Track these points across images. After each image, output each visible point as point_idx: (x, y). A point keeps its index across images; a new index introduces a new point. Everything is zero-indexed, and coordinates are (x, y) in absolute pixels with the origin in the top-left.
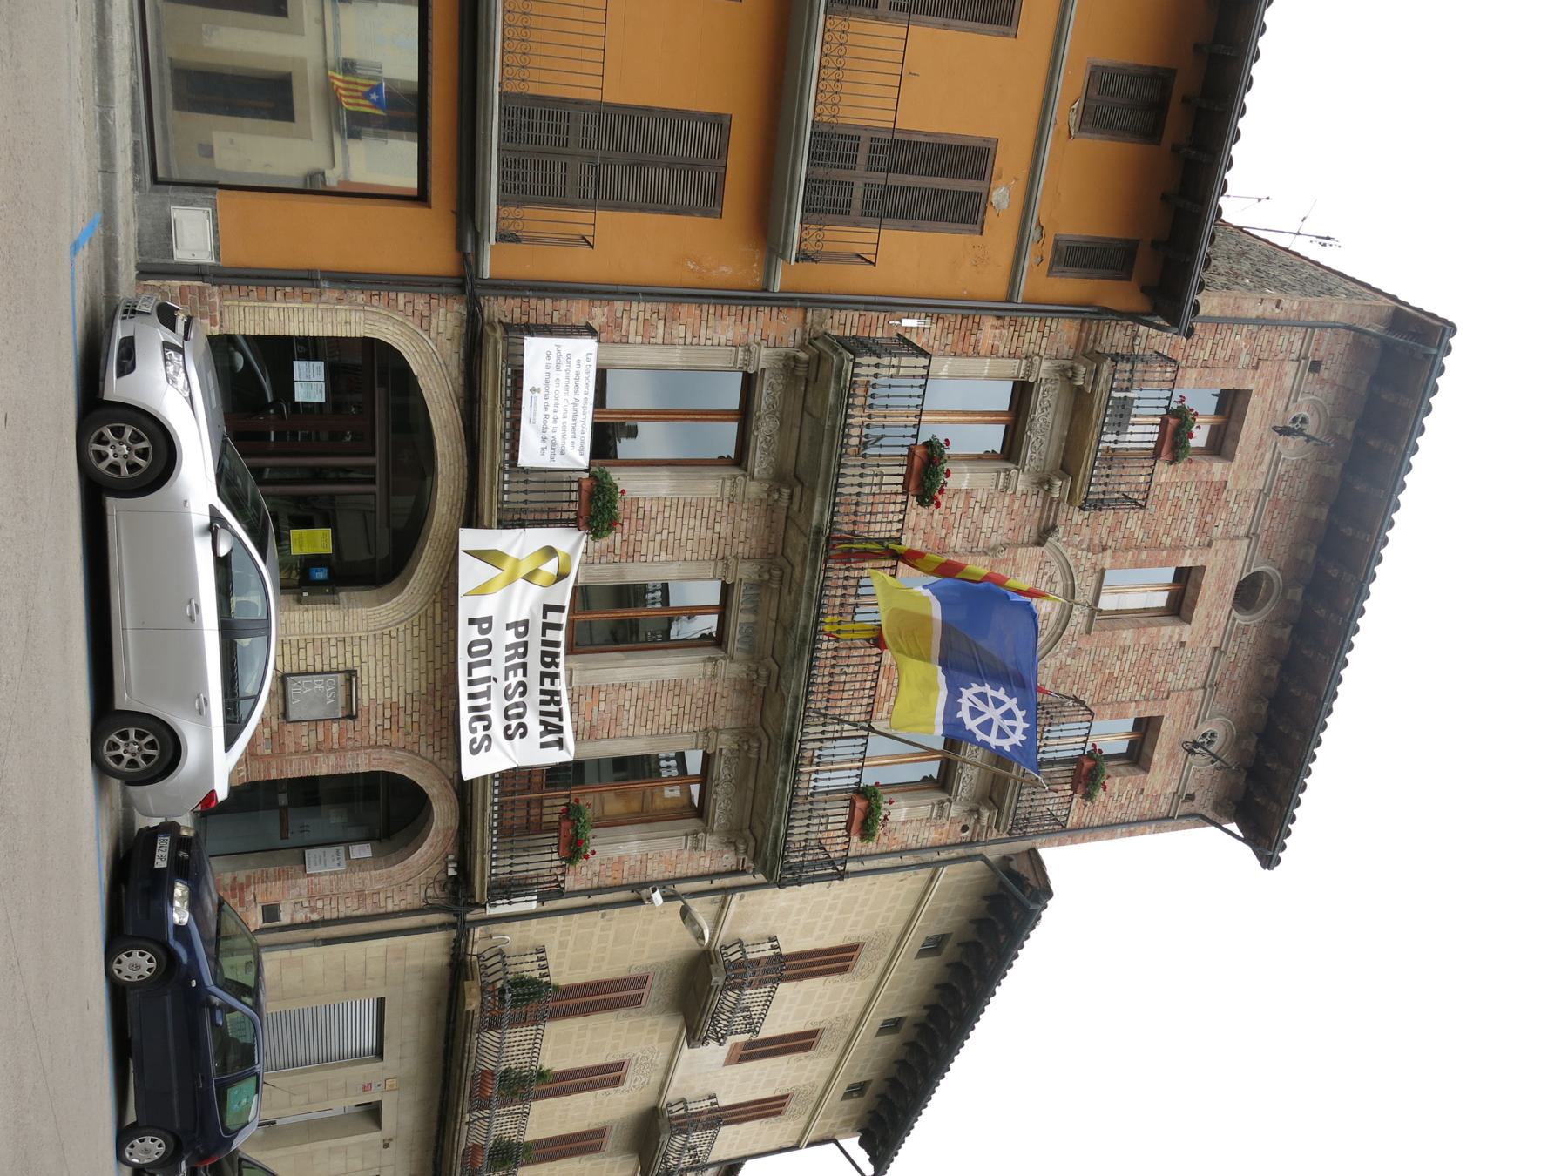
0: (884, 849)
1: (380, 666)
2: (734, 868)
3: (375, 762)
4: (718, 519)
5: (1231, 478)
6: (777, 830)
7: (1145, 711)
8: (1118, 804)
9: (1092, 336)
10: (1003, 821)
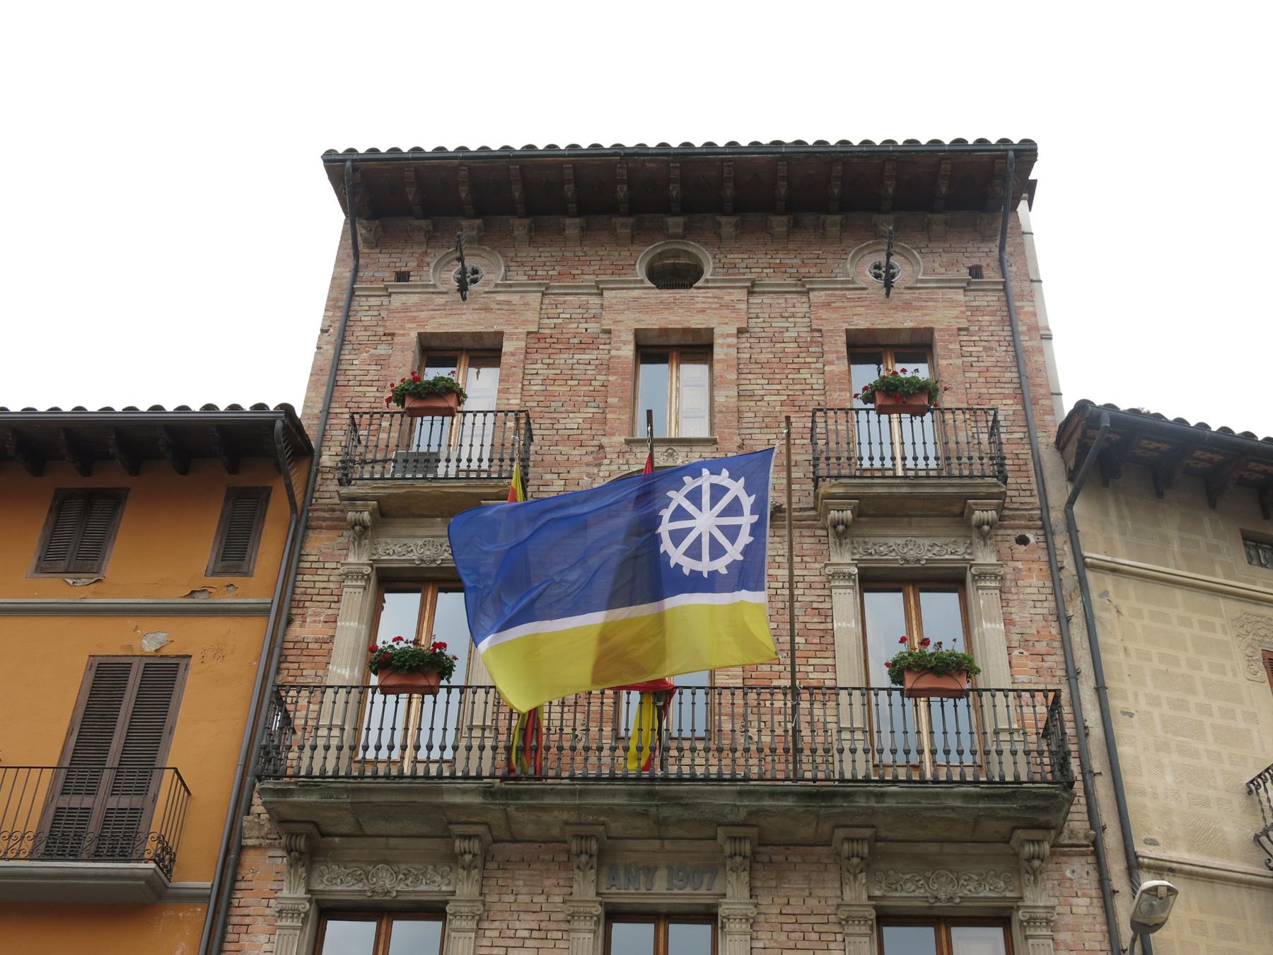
0: (1057, 644)
2: (1091, 859)
4: (511, 933)
5: (523, 330)
6: (967, 797)
8: (984, 354)
9: (326, 515)
10: (984, 490)
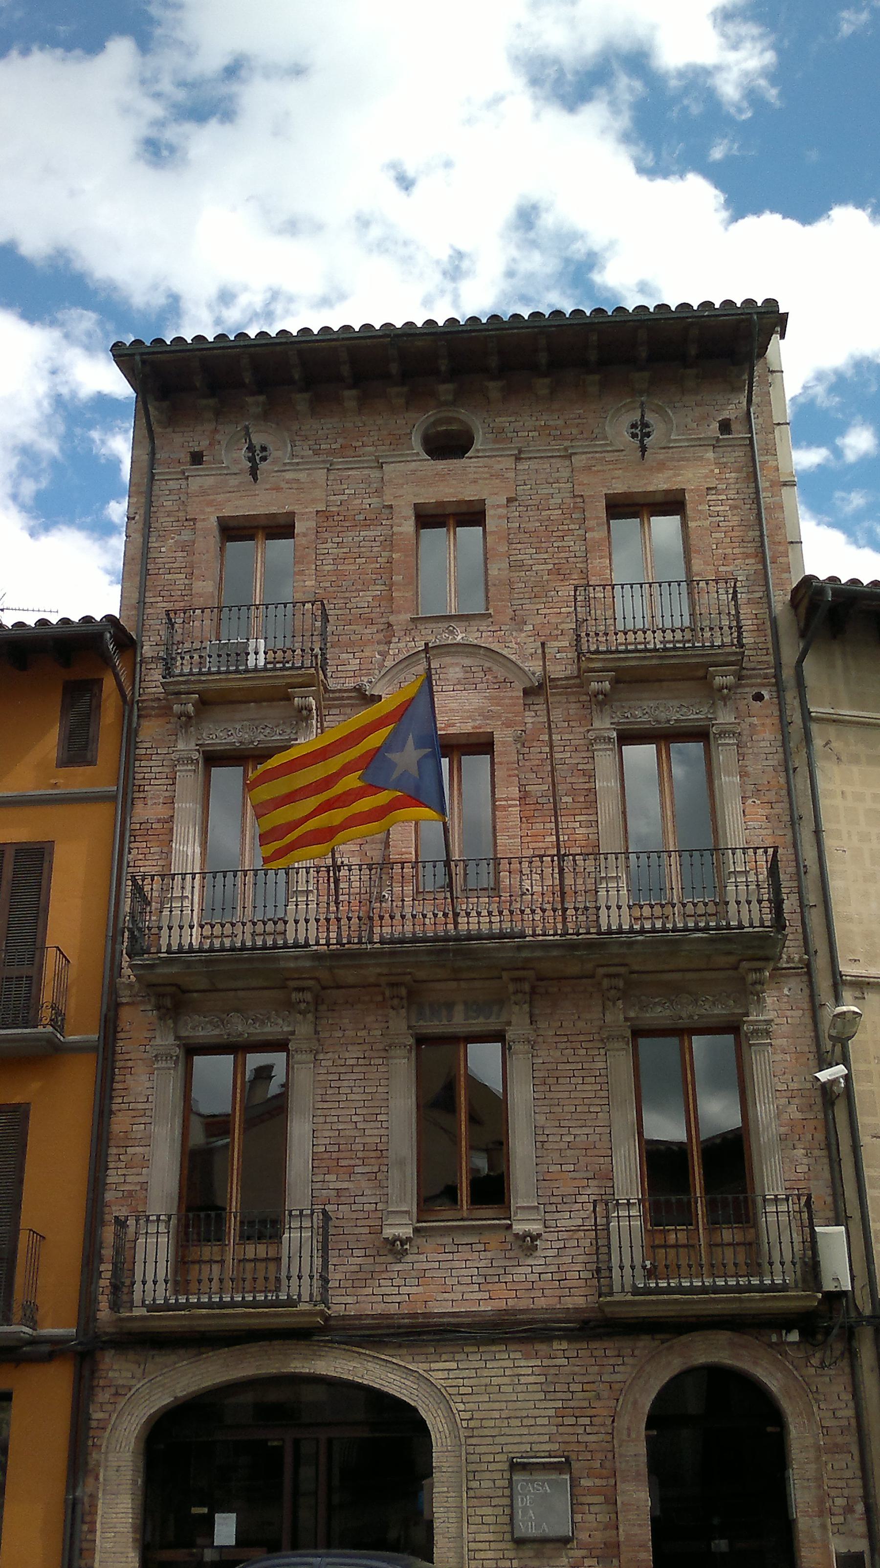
1: (507, 1431)
3: (633, 1435)
4: (342, 1062)
5: (311, 509)
7: (598, 518)
